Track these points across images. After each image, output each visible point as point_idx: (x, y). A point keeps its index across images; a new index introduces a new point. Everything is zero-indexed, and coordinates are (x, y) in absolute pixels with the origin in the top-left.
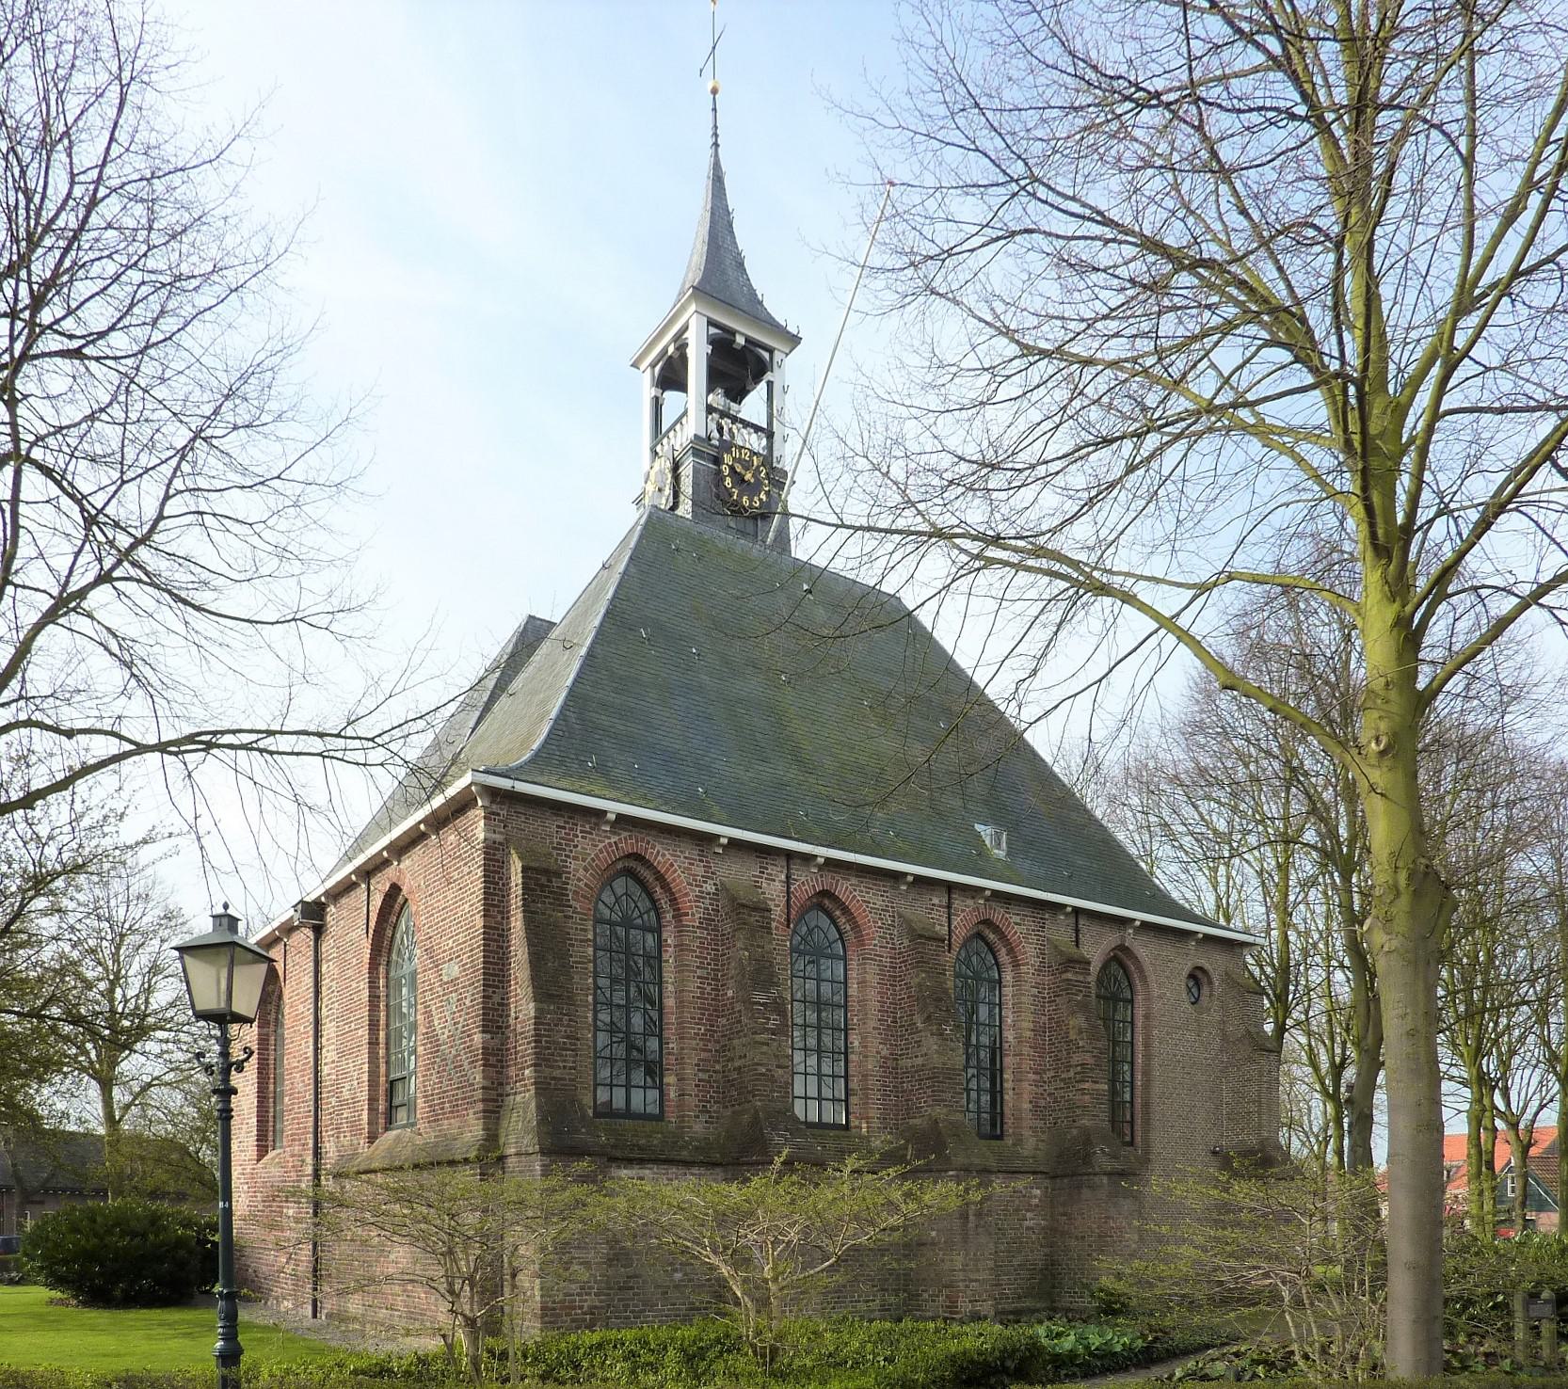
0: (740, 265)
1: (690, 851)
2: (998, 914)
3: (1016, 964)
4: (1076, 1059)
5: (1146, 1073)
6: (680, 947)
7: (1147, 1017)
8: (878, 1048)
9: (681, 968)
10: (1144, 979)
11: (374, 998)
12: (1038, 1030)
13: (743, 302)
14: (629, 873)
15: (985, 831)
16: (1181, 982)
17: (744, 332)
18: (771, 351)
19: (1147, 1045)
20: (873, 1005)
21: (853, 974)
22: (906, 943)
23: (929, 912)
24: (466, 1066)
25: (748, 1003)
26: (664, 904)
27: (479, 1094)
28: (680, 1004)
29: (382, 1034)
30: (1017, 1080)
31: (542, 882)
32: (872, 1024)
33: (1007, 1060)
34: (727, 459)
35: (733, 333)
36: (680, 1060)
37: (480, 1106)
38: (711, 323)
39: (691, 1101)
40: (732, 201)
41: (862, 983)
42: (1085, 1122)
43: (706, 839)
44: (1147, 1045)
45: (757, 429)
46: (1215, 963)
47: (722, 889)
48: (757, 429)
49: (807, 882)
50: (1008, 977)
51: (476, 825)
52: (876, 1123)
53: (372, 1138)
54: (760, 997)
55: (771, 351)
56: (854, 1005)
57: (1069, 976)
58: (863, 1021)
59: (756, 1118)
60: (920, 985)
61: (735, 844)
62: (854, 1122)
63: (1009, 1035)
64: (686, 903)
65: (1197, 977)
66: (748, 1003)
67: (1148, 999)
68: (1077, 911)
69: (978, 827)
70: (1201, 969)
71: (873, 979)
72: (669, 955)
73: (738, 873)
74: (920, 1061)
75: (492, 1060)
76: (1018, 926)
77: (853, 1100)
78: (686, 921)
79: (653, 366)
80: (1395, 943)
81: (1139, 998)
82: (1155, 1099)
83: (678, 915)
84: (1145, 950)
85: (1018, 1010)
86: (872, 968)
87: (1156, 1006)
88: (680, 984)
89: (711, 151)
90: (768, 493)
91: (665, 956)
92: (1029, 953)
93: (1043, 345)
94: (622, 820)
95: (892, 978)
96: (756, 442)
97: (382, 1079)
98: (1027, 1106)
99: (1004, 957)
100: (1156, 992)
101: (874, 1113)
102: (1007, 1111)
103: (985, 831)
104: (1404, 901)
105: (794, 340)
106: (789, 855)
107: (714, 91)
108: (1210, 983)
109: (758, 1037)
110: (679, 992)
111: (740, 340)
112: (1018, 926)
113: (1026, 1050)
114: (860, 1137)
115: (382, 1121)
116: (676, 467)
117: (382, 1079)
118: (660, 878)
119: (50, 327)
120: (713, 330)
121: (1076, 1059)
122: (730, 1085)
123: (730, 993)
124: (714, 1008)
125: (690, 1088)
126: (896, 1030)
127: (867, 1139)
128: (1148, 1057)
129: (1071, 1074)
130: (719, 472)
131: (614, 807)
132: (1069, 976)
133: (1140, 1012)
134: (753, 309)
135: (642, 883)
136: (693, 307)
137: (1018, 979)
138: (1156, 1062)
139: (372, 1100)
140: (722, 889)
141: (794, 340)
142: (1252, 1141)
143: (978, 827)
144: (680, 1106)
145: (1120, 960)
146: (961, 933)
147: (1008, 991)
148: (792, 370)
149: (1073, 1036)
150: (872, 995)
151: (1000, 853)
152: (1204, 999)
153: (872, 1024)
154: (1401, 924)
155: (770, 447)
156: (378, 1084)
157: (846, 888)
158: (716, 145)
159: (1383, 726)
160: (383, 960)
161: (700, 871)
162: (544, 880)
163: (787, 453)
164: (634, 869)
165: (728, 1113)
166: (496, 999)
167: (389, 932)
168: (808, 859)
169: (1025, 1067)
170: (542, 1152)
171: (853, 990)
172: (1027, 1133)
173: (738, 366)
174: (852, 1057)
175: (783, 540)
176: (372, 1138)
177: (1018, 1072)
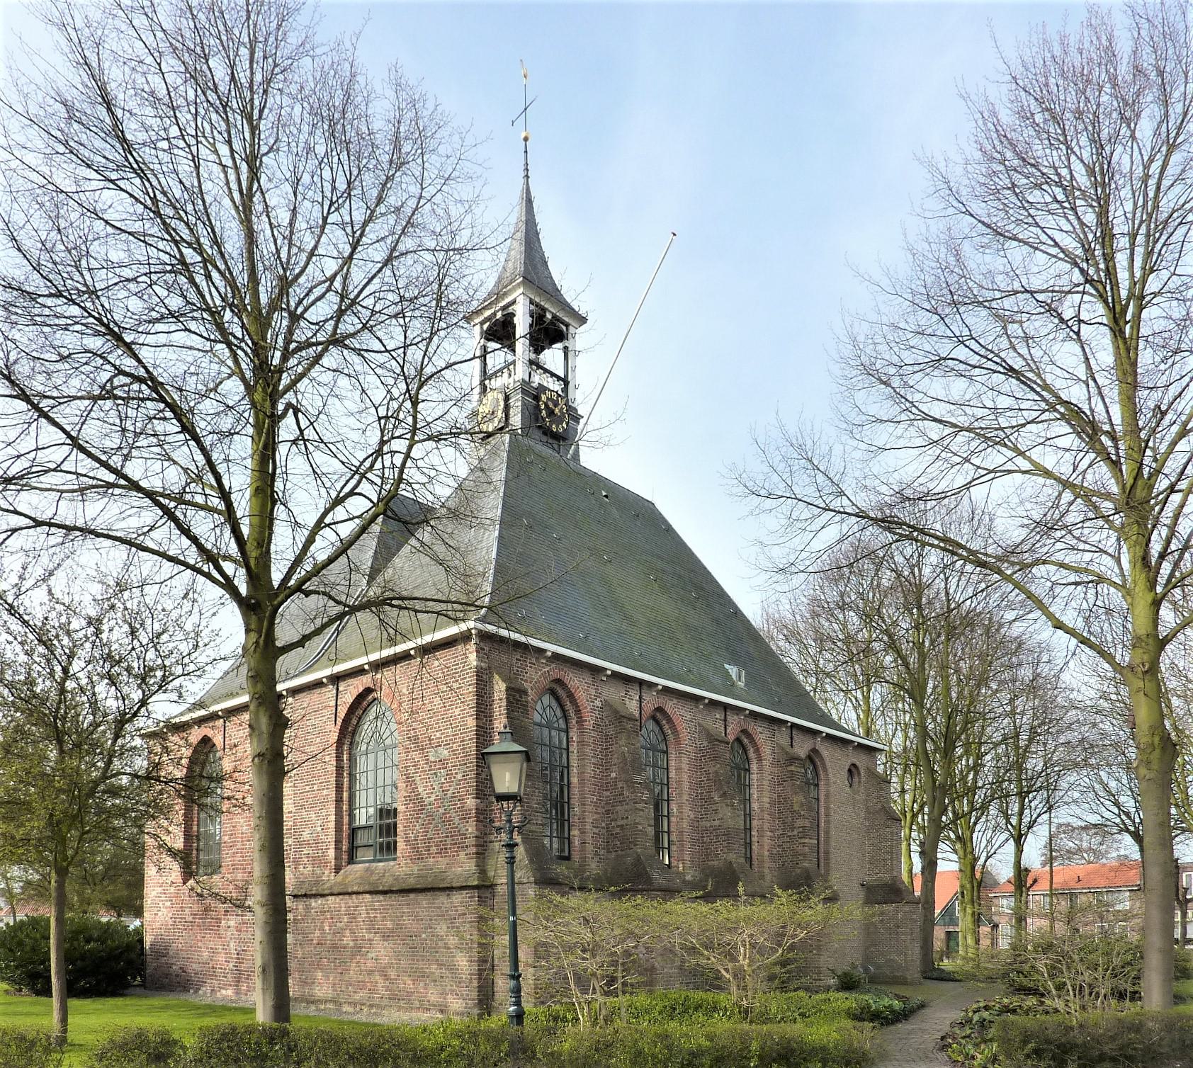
0: (545, 263)
1: (588, 678)
2: (751, 726)
3: (760, 760)
4: (799, 823)
5: (827, 833)
6: (581, 743)
7: (827, 796)
8: (688, 813)
9: (582, 757)
10: (825, 770)
11: (339, 769)
12: (772, 804)
13: (550, 289)
14: (553, 693)
15: (733, 670)
16: (845, 774)
17: (552, 310)
18: (567, 325)
19: (827, 815)
20: (686, 785)
21: (672, 763)
22: (705, 743)
23: (714, 721)
24: (457, 821)
25: (631, 783)
26: (572, 713)
27: (473, 841)
28: (582, 781)
29: (345, 795)
30: (761, 836)
31: (516, 697)
32: (686, 797)
33: (755, 823)
34: (544, 398)
35: (544, 310)
36: (582, 819)
37: (474, 850)
38: (532, 302)
39: (589, 848)
40: (538, 218)
41: (679, 769)
42: (806, 864)
43: (595, 670)
44: (827, 815)
45: (559, 378)
46: (861, 760)
47: (606, 704)
48: (559, 378)
49: (651, 701)
50: (754, 767)
51: (470, 656)
52: (688, 864)
53: (338, 869)
54: (637, 779)
55: (567, 325)
56: (673, 784)
57: (793, 768)
58: (680, 795)
59: (638, 859)
60: (716, 772)
61: (616, 675)
62: (674, 863)
63: (755, 806)
64: (586, 713)
65: (852, 771)
66: (631, 783)
67: (827, 784)
68: (794, 726)
69: (727, 666)
70: (854, 765)
71: (685, 767)
72: (574, 747)
73: (613, 693)
74: (717, 823)
75: (482, 817)
76: (761, 733)
77: (674, 848)
78: (586, 725)
79: (482, 323)
80: (1152, 775)
81: (822, 783)
82: (832, 850)
83: (581, 721)
84: (826, 751)
85: (760, 791)
86: (685, 760)
87: (832, 789)
88: (582, 767)
89: (522, 181)
90: (567, 424)
91: (571, 749)
92: (767, 751)
93: (966, 434)
94: (557, 657)
95: (697, 766)
96: (556, 386)
97: (345, 827)
98: (766, 853)
99: (752, 755)
100: (832, 779)
101: (687, 857)
102: (754, 856)
103: (733, 670)
104: (1157, 751)
105: (583, 320)
106: (641, 682)
107: (526, 139)
108: (859, 774)
109: (638, 806)
110: (581, 774)
111: (549, 316)
112: (761, 733)
113: (766, 817)
114: (678, 873)
115: (345, 857)
116: (507, 398)
117: (345, 827)
118: (571, 696)
119: (387, 351)
120: (533, 307)
121: (799, 823)
122: (615, 838)
123: (613, 775)
124: (604, 785)
125: (589, 839)
126: (703, 802)
127: (683, 874)
128: (828, 822)
129: (795, 833)
130: (538, 406)
131: (551, 648)
132: (793, 768)
133: (822, 793)
134: (553, 293)
135: (558, 699)
136: (521, 290)
137: (760, 770)
138: (832, 825)
139: (338, 842)
140: (606, 704)
141: (583, 320)
142: (887, 878)
143: (727, 666)
144: (583, 850)
145: (813, 758)
146: (731, 738)
147: (754, 777)
148: (581, 338)
149: (796, 808)
150: (685, 777)
151: (741, 684)
152: (855, 784)
153: (686, 797)
154: (1155, 765)
155: (565, 389)
156: (342, 831)
157: (671, 706)
158: (527, 176)
159: (1146, 657)
160: (347, 741)
161: (593, 692)
162: (518, 697)
163: (581, 400)
164: (557, 690)
165: (613, 855)
166: (484, 776)
167: (354, 721)
168: (652, 685)
169: (765, 828)
170: (536, 883)
171: (673, 774)
172: (766, 871)
173: (550, 331)
174: (673, 819)
175: (576, 456)
176: (338, 869)
177: (761, 831)
